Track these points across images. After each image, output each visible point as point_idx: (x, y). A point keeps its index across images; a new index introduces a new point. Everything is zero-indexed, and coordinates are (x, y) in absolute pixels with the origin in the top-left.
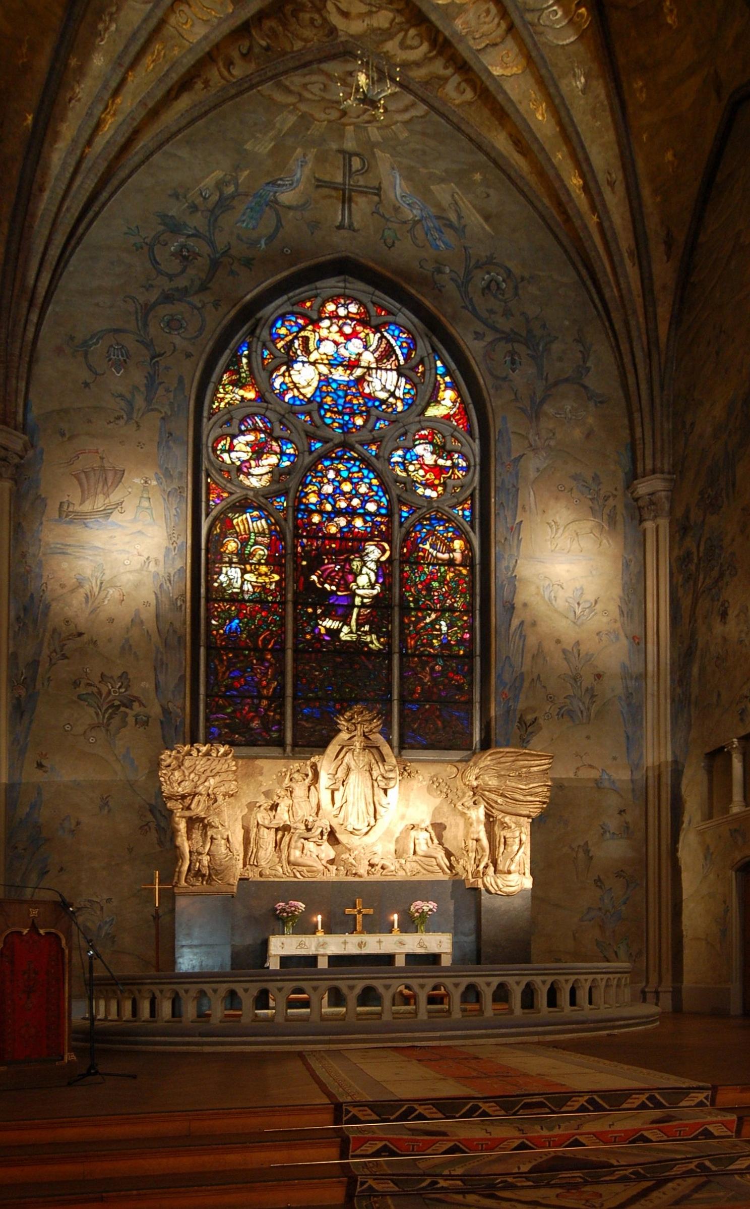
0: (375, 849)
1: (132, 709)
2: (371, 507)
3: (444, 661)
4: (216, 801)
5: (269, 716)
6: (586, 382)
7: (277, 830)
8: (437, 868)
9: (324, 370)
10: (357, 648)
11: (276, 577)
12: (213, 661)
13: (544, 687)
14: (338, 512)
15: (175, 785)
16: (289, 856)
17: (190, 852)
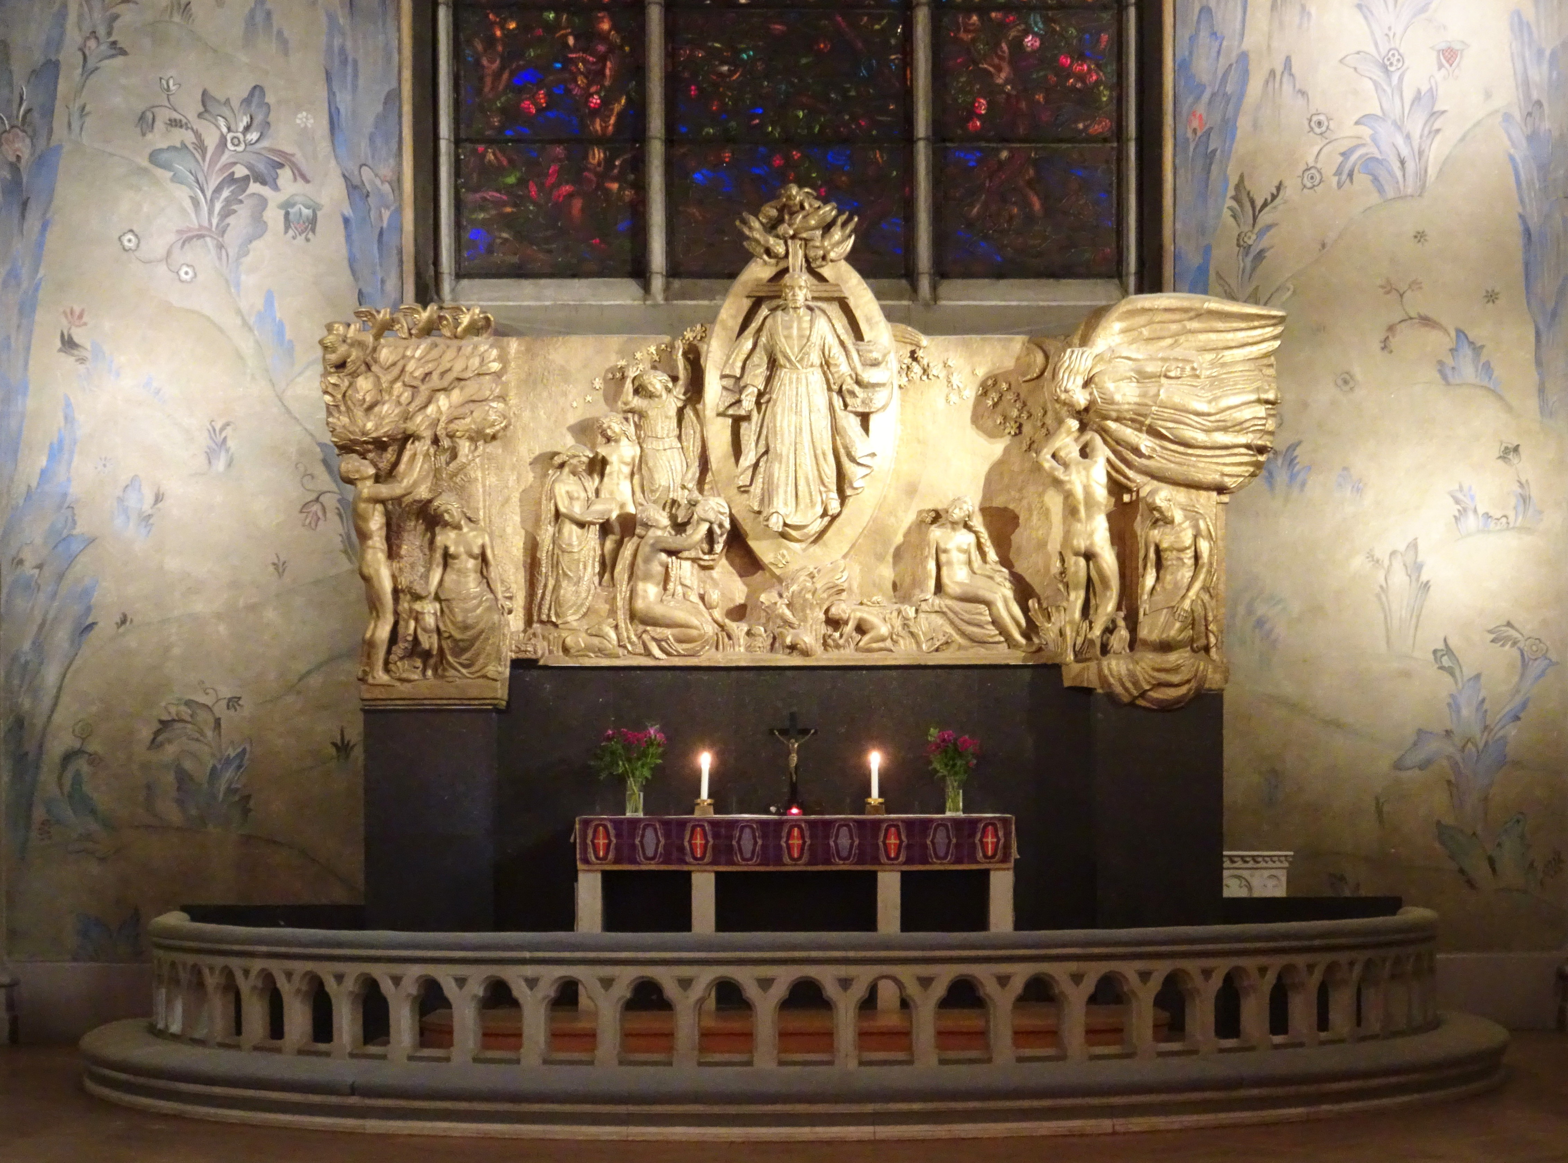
0: (841, 579)
1: (276, 188)
3: (1047, 21)
4: (454, 456)
5: (607, 192)
7: (605, 529)
8: (992, 630)
12: (469, 42)
13: (1303, 93)
15: (359, 413)
16: (631, 598)
17: (396, 592)
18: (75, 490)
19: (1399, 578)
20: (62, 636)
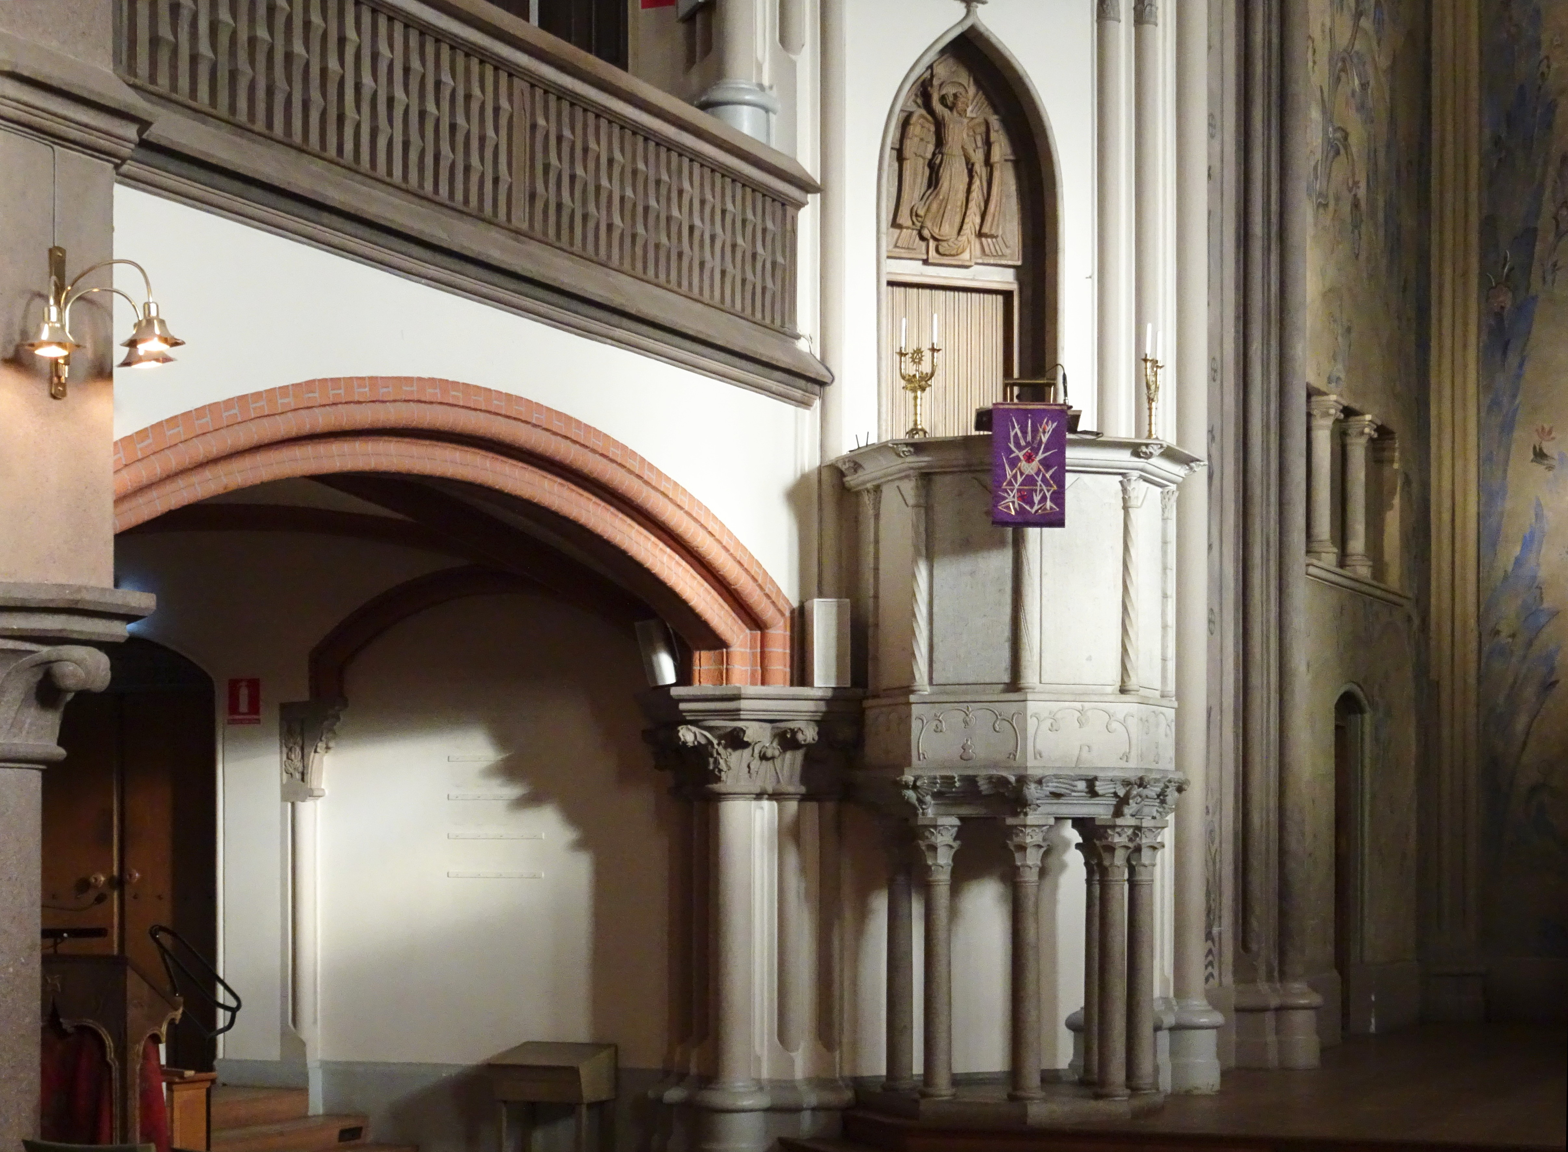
18: (1543, 573)
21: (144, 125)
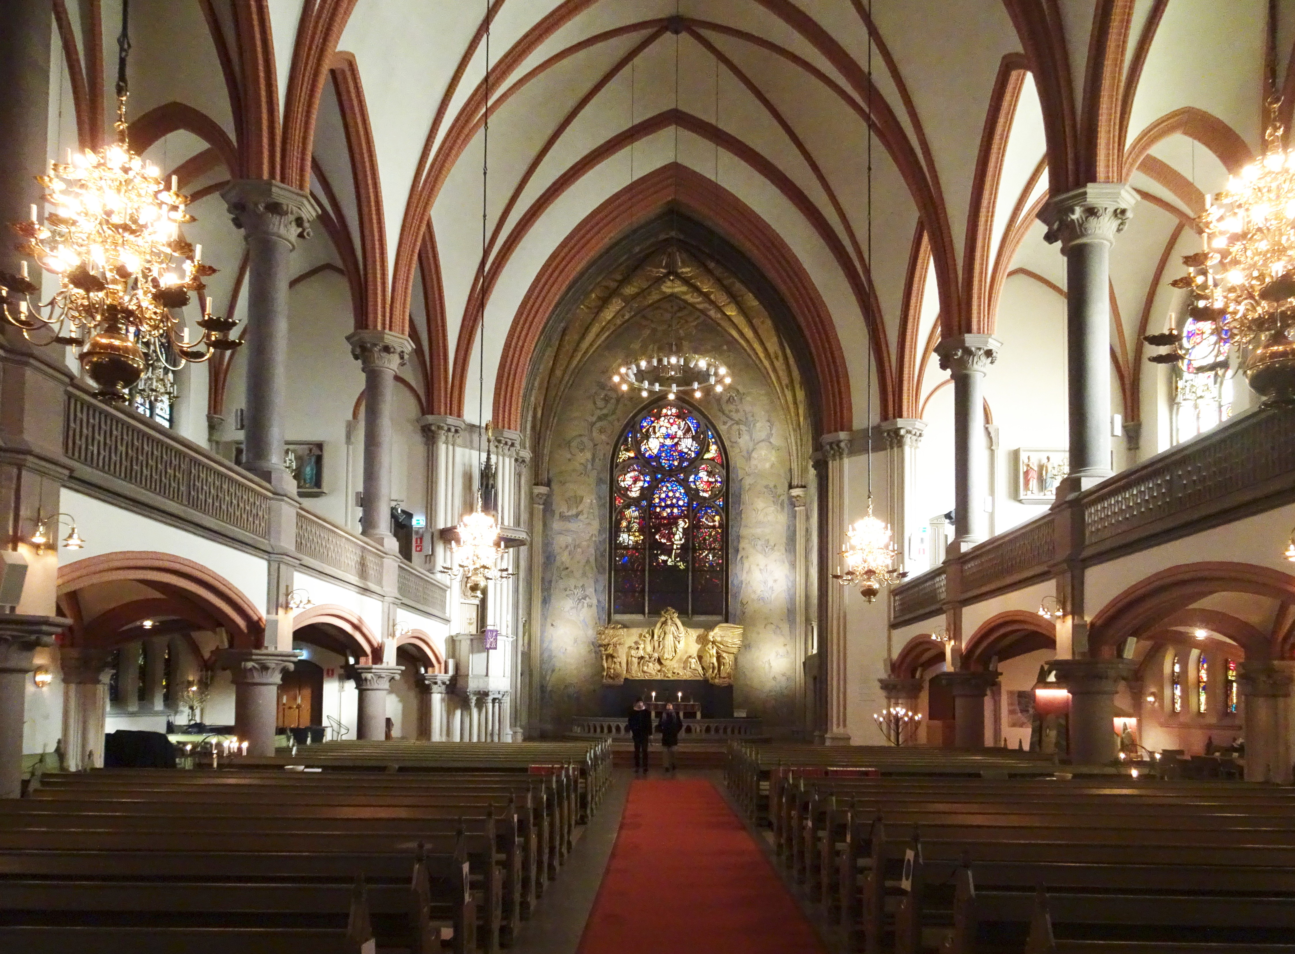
2: (681, 503)
6: (772, 440)
9: (662, 440)
10: (675, 567)
11: (642, 537)
14: (667, 506)
19: (767, 665)
20: (549, 672)
21: (71, 470)
